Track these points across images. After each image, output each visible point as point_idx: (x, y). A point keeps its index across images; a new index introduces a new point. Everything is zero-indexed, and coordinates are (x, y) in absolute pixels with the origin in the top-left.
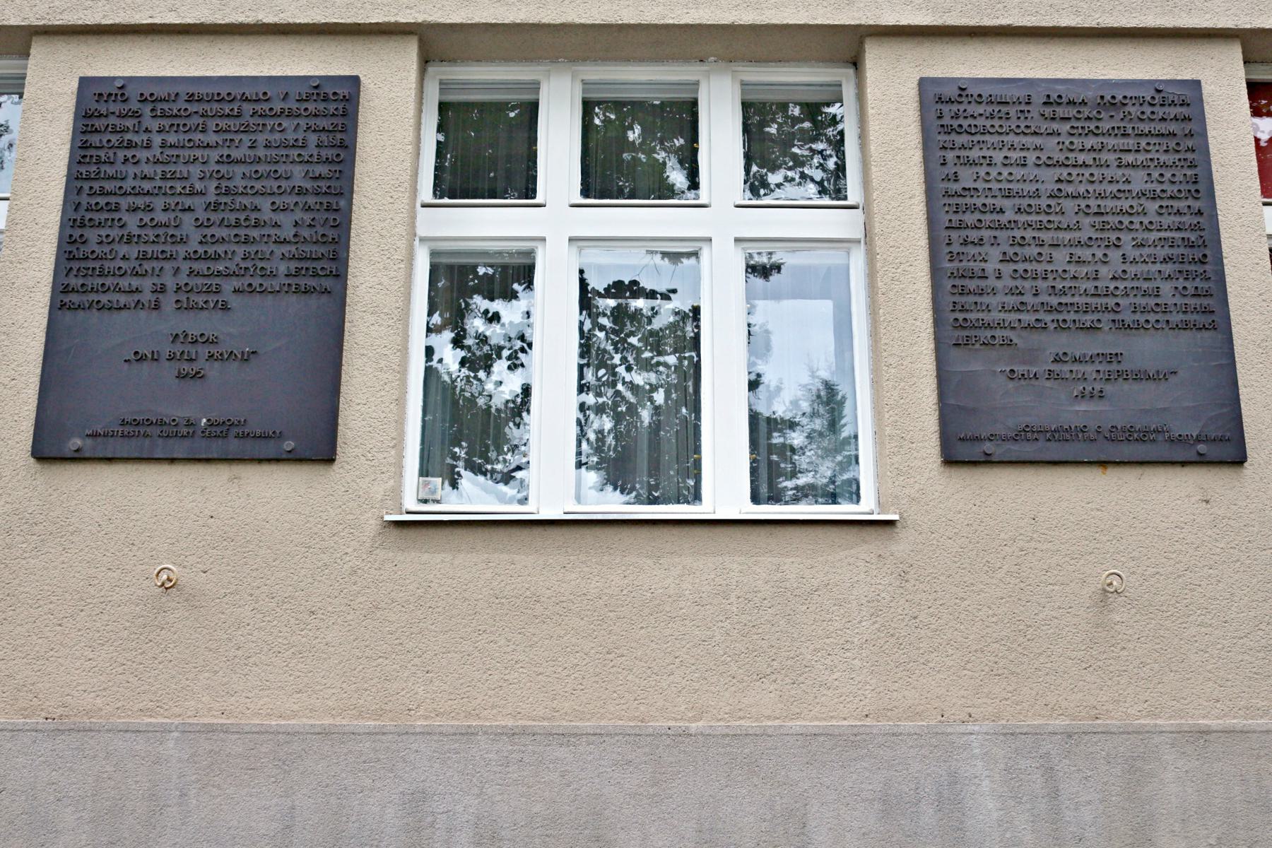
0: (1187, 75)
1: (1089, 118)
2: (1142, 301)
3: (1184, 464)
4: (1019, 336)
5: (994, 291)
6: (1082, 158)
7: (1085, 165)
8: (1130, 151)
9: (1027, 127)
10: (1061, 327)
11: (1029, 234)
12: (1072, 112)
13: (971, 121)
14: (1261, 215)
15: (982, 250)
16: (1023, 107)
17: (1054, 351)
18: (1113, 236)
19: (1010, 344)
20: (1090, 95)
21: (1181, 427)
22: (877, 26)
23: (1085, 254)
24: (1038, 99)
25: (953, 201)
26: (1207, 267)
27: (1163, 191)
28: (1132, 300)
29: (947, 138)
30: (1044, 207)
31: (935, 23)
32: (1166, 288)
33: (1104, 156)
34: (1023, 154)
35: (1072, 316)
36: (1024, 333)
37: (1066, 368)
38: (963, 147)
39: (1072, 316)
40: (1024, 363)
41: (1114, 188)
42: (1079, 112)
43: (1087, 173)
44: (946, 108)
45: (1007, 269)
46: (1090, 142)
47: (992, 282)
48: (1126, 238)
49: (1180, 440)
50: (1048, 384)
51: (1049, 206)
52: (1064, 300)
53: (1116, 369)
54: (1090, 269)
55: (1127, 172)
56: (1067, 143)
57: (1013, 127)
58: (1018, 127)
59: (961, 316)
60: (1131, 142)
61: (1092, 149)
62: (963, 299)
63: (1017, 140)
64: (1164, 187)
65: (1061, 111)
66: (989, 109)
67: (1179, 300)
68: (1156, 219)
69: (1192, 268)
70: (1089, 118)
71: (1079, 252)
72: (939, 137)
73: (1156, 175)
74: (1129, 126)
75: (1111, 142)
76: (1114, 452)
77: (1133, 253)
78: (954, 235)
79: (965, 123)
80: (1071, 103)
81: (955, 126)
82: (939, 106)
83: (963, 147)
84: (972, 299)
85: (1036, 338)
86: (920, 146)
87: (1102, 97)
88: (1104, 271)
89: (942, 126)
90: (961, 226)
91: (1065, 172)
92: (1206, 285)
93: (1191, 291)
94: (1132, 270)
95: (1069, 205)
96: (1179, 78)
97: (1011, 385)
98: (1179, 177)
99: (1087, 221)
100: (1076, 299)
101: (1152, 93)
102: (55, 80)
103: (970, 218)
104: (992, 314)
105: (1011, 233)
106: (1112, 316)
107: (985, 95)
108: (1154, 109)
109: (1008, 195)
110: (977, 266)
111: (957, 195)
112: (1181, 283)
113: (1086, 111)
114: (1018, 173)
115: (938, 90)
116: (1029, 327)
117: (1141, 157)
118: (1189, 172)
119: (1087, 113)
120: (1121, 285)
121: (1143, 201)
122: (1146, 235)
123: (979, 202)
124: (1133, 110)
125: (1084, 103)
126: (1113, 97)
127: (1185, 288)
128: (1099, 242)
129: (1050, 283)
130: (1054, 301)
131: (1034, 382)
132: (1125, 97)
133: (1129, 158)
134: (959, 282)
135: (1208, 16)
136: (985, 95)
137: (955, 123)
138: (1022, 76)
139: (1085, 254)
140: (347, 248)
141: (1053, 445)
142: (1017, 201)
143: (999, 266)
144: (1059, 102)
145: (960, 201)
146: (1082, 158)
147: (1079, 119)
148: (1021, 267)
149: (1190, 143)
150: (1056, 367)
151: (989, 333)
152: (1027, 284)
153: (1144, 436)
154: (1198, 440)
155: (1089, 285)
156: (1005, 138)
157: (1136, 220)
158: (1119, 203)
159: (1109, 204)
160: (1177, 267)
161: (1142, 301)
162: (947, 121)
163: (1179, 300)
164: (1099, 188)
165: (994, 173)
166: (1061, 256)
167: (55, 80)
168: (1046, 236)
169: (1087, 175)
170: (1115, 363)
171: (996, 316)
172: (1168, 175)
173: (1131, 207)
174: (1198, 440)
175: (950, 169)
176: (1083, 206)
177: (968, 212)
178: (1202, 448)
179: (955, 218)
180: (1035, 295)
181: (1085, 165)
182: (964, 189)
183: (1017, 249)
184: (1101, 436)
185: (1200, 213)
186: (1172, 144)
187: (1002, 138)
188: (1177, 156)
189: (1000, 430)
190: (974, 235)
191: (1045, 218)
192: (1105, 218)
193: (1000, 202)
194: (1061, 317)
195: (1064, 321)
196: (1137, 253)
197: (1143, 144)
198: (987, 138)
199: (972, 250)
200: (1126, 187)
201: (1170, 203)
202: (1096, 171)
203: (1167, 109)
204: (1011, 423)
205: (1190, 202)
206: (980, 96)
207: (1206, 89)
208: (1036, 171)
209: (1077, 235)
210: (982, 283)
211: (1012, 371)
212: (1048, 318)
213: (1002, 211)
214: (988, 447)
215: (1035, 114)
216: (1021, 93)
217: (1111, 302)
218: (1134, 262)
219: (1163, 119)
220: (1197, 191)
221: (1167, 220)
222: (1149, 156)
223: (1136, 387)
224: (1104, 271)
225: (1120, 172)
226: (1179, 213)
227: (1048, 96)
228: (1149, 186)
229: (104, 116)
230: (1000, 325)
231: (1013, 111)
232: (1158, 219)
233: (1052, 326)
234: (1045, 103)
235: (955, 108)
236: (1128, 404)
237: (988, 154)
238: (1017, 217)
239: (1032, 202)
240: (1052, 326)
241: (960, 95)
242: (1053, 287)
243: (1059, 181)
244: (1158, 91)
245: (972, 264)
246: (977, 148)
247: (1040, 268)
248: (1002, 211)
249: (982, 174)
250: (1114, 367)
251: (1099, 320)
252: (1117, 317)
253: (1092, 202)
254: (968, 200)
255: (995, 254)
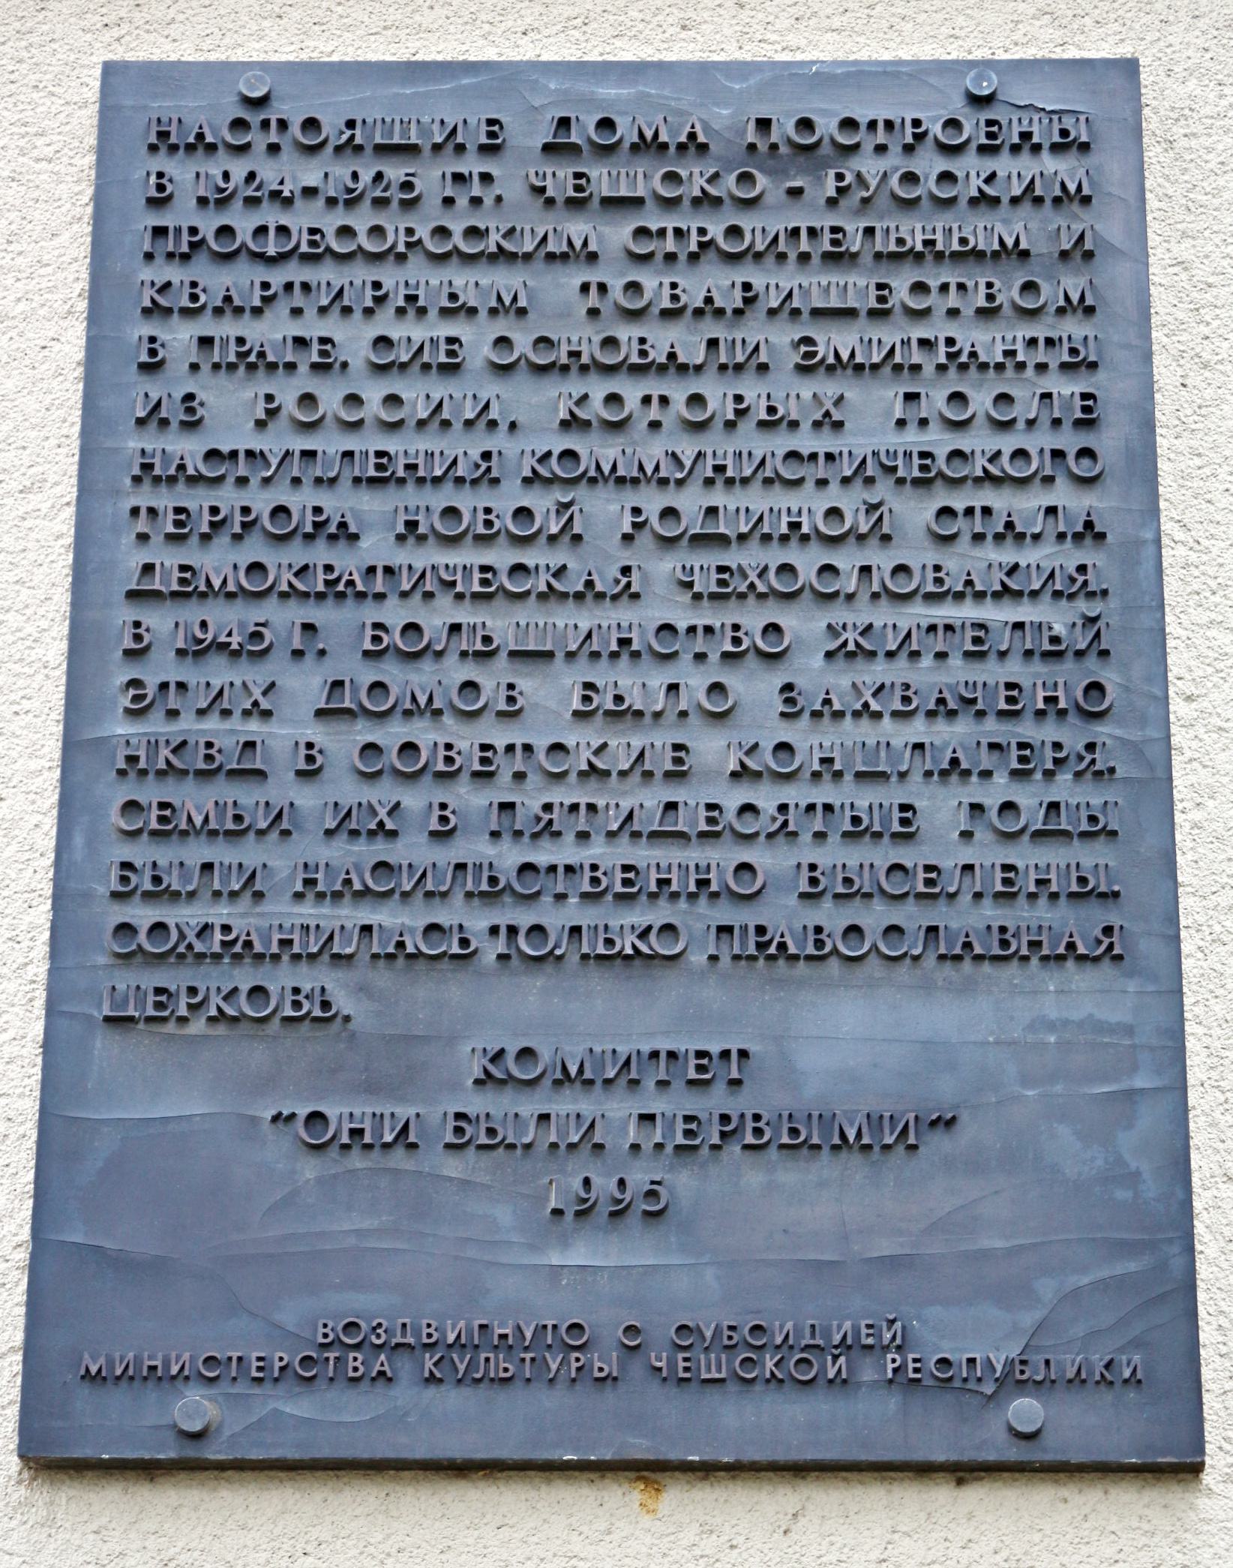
2: (834, 855)
3: (963, 1472)
4: (363, 989)
5: (280, 824)
6: (663, 338)
7: (674, 366)
9: (473, 232)
10: (533, 954)
12: (642, 179)
16: (472, 165)
20: (724, 118)
21: (979, 1334)
23: (640, 684)
24: (528, 135)
25: (165, 500)
26: (1102, 731)
28: (808, 853)
29: (175, 274)
32: (941, 807)
33: (754, 331)
34: (446, 329)
35: (574, 913)
36: (383, 978)
39: (574, 913)
40: (371, 1088)
41: (781, 443)
43: (678, 392)
44: (182, 172)
45: (341, 744)
46: (718, 282)
48: (803, 625)
49: (948, 1380)
50: (453, 1167)
52: (543, 856)
54: (662, 739)
55: (828, 388)
59: (143, 916)
61: (709, 309)
62: (165, 854)
63: (431, 281)
65: (603, 179)
67: (987, 854)
69: (1047, 733)
70: (705, 201)
71: (608, 677)
72: (147, 274)
74: (854, 227)
76: (672, 1424)
78: (159, 621)
80: (648, 146)
82: (161, 162)
83: (228, 307)
84: (196, 852)
85: (430, 997)
87: (764, 124)
88: (713, 749)
90: (190, 588)
92: (1092, 796)
93: (1031, 814)
94: (810, 741)
95: (604, 511)
96: (1072, 53)
97: (310, 1169)
98: (1026, 407)
99: (665, 566)
100: (597, 851)
101: (957, 107)
103: (218, 561)
105: (371, 613)
106: (726, 913)
107: (331, 127)
108: (956, 166)
110: (226, 733)
111: (181, 475)
112: (998, 790)
115: (164, 106)
118: (1066, 388)
120: (766, 797)
125: (694, 146)
128: (700, 644)
129: (502, 790)
130: (508, 857)
131: (399, 1158)
132: (848, 124)
133: (841, 340)
134: (150, 793)
138: (490, 54)
139: (640, 684)
141: (451, 1399)
142: (411, 497)
143: (316, 733)
145: (198, 500)
146: (663, 338)
148: (391, 735)
149: (1073, 284)
151: (245, 978)
153: (806, 1364)
154: (1015, 1379)
156: (391, 277)
157: (846, 560)
159: (742, 505)
160: (993, 729)
161: (834, 855)
162: (182, 215)
163: (987, 854)
164: (718, 445)
166: (550, 694)
168: (503, 624)
170: (720, 1088)
172: (981, 401)
174: (1015, 1379)
175: (173, 385)
177: (223, 540)
179: (169, 559)
182: (212, 455)
183: (391, 672)
184: (637, 1368)
185: (1090, 532)
188: (1025, 331)
189: (241, 1339)
190: (227, 620)
191: (501, 557)
192: (732, 558)
194: (524, 919)
196: (841, 681)
197: (901, 283)
199: (219, 673)
200: (823, 443)
201: (987, 497)
204: (290, 1315)
205: (1062, 495)
210: (247, 796)
212: (478, 921)
213: (345, 535)
217: (723, 857)
218: (827, 712)
219: (983, 201)
221: (970, 561)
222: (920, 331)
223: (791, 1174)
224: (713, 749)
225: (807, 389)
228: (913, 439)
231: (430, 178)
233: (490, 951)
236: (772, 1231)
237: (313, 328)
238: (400, 557)
240: (490, 951)
241: (239, 124)
242: (507, 807)
243: (571, 423)
245: (212, 723)
246: (282, 307)
251: (668, 928)
253: (691, 502)
254: (228, 498)
255: (305, 686)
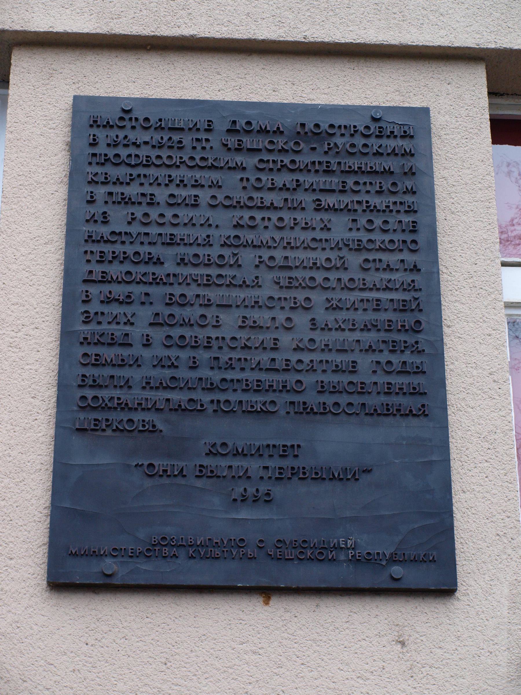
0: (416, 103)
1: (283, 151)
5: (137, 363)
6: (269, 197)
7: (272, 207)
8: (333, 191)
9: (203, 159)
10: (224, 410)
11: (191, 291)
12: (262, 142)
13: (132, 150)
14: (498, 275)
15: (128, 310)
16: (203, 136)
17: (211, 440)
18: (301, 296)
19: (154, 430)
22: (25, 32)
23: (262, 316)
24: (221, 126)
25: (96, 248)
27: (370, 241)
30: (215, 258)
31: (99, 31)
32: (365, 362)
36: (174, 417)
37: (224, 463)
38: (118, 182)
41: (308, 235)
42: (271, 142)
43: (274, 217)
44: (101, 134)
45: (158, 335)
47: (138, 350)
48: (318, 298)
49: (369, 561)
50: (199, 483)
51: (221, 257)
52: (229, 375)
53: (293, 468)
55: (326, 216)
56: (252, 179)
57: (185, 158)
58: (192, 158)
59: (90, 393)
60: (335, 180)
61: (284, 188)
64: (372, 237)
65: (248, 142)
66: (157, 137)
67: (382, 379)
68: (358, 276)
69: (401, 337)
70: (283, 151)
71: (255, 315)
72: (89, 169)
73: (363, 221)
75: (308, 179)
77: (322, 315)
78: (94, 290)
79: (124, 153)
81: (111, 155)
82: (94, 131)
83: (118, 182)
84: (108, 371)
85: (189, 425)
86: (66, 180)
87: (303, 125)
89: (94, 155)
90: (105, 279)
91: (247, 214)
92: (417, 360)
97: (148, 483)
102: (46, 96)
103: (115, 270)
104: (133, 391)
105: (168, 290)
107: (153, 120)
109: (171, 242)
110: (118, 330)
111: (102, 240)
113: (280, 142)
114: (185, 214)
116: (179, 409)
117: (346, 199)
119: (281, 144)
120: (306, 358)
121: (345, 252)
122: (344, 295)
123: (130, 250)
124: (340, 141)
126: (317, 126)
127: (389, 363)
128: (283, 304)
130: (216, 376)
132: (332, 126)
133: (331, 200)
134: (92, 350)
135: (442, 33)
136: (153, 120)
137: (111, 152)
139: (262, 316)
140: (66, 334)
142: (181, 250)
143: (149, 331)
144: (250, 132)
145: (107, 248)
146: (269, 197)
147: (270, 151)
148: (176, 332)
149: (409, 184)
150: (207, 462)
151: (125, 416)
152: (184, 355)
154: (393, 560)
155: (265, 357)
156: (174, 173)
157: (333, 276)
158: (312, 255)
160: (383, 335)
163: (382, 379)
165: (154, 214)
166: (230, 320)
167: (46, 96)
168: (213, 294)
169: (274, 218)
171: (137, 394)
172: (378, 222)
173: (328, 260)
175: (98, 209)
176: (265, 257)
178: (397, 570)
179: (98, 269)
180: (191, 368)
181: (272, 207)
182: (113, 233)
186: (387, 185)
187: (168, 172)
188: (393, 199)
190: (119, 290)
191: (214, 272)
192: (294, 274)
193: (156, 251)
194: (222, 397)
195: (227, 401)
196: (331, 318)
197: (350, 182)
198: (152, 171)
199: (116, 309)
200: (324, 235)
201: (378, 256)
202: (287, 216)
203: (384, 142)
206: (147, 119)
207: (438, 120)
208: (209, 213)
209: (256, 292)
210: (125, 352)
211: (151, 465)
212: (206, 398)
214: (109, 565)
215: (215, 143)
216: (201, 119)
217: (292, 378)
218: (326, 328)
220: (414, 242)
222: (356, 198)
225: (318, 216)
226: (388, 268)
227: (234, 122)
228: (355, 235)
229: (113, 150)
230: (140, 407)
231: (187, 140)
232: (361, 276)
233: (210, 408)
234: (228, 131)
235: (112, 133)
236: (302, 508)
238: (178, 270)
239: (200, 251)
240: (210, 408)
241: (121, 119)
242: (217, 359)
243: (237, 226)
244: (375, 120)
245: (114, 326)
247: (202, 334)
248: (159, 262)
249: (139, 215)
250: (286, 463)
251: (273, 402)
252: (296, 398)
253: (279, 254)
254: (119, 248)
255: (145, 314)
